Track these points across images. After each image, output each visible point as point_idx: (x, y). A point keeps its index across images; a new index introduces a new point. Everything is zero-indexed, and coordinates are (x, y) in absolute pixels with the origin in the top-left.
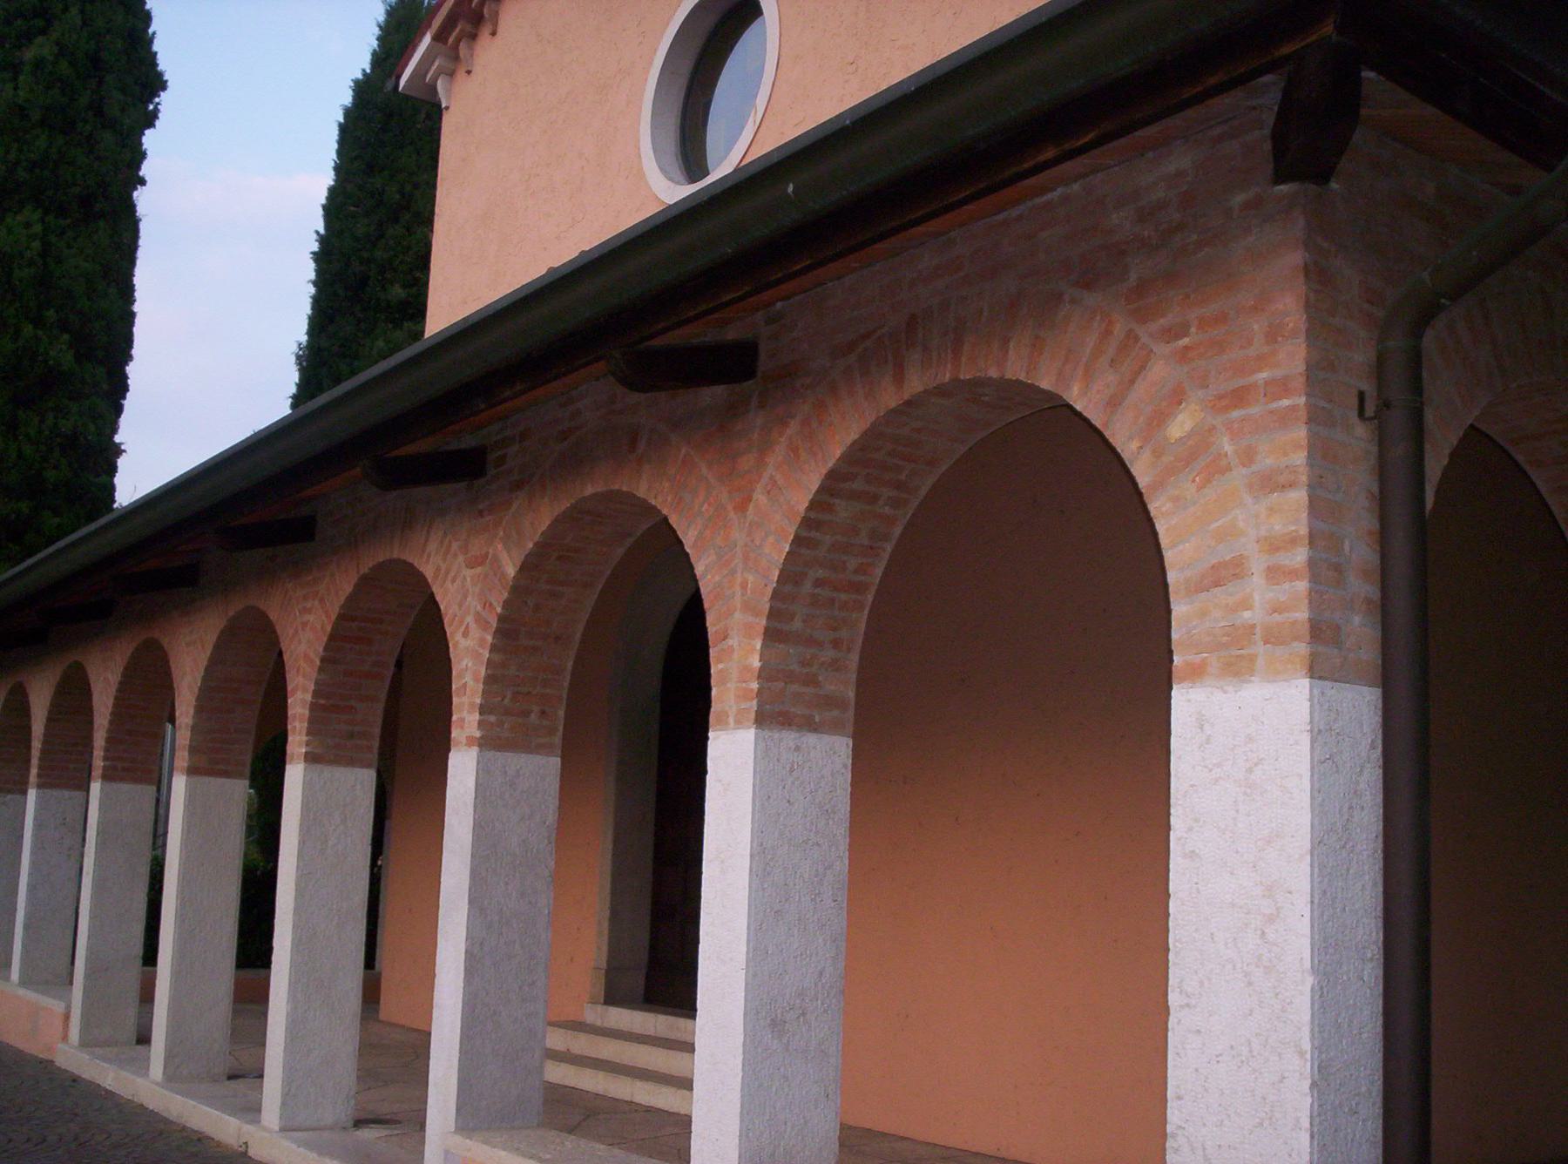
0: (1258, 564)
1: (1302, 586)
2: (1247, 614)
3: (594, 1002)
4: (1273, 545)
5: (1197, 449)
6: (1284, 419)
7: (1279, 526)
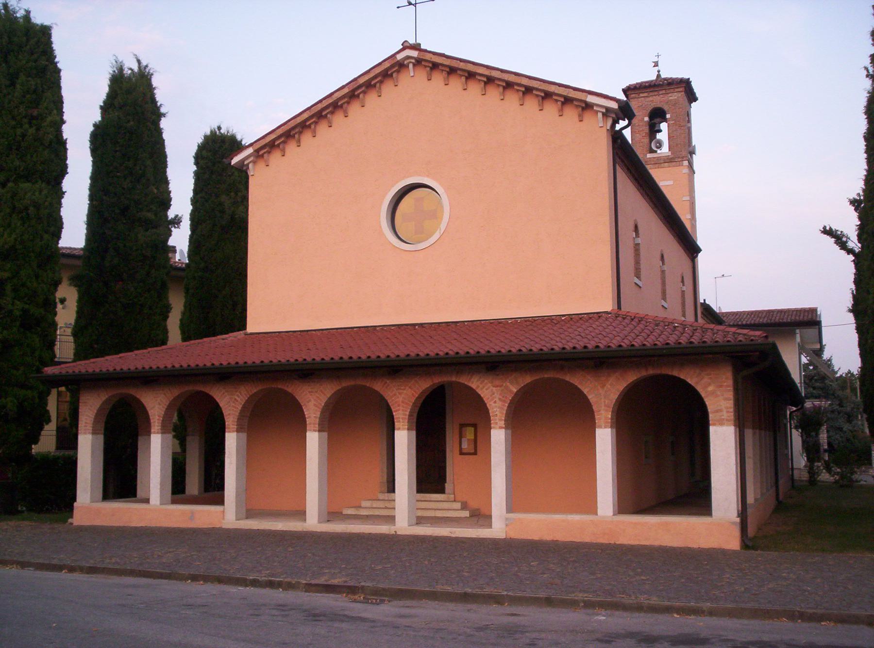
0: (725, 410)
1: (732, 414)
2: (723, 417)
3: (382, 492)
4: (727, 408)
5: (713, 393)
6: (729, 391)
7: (728, 405)
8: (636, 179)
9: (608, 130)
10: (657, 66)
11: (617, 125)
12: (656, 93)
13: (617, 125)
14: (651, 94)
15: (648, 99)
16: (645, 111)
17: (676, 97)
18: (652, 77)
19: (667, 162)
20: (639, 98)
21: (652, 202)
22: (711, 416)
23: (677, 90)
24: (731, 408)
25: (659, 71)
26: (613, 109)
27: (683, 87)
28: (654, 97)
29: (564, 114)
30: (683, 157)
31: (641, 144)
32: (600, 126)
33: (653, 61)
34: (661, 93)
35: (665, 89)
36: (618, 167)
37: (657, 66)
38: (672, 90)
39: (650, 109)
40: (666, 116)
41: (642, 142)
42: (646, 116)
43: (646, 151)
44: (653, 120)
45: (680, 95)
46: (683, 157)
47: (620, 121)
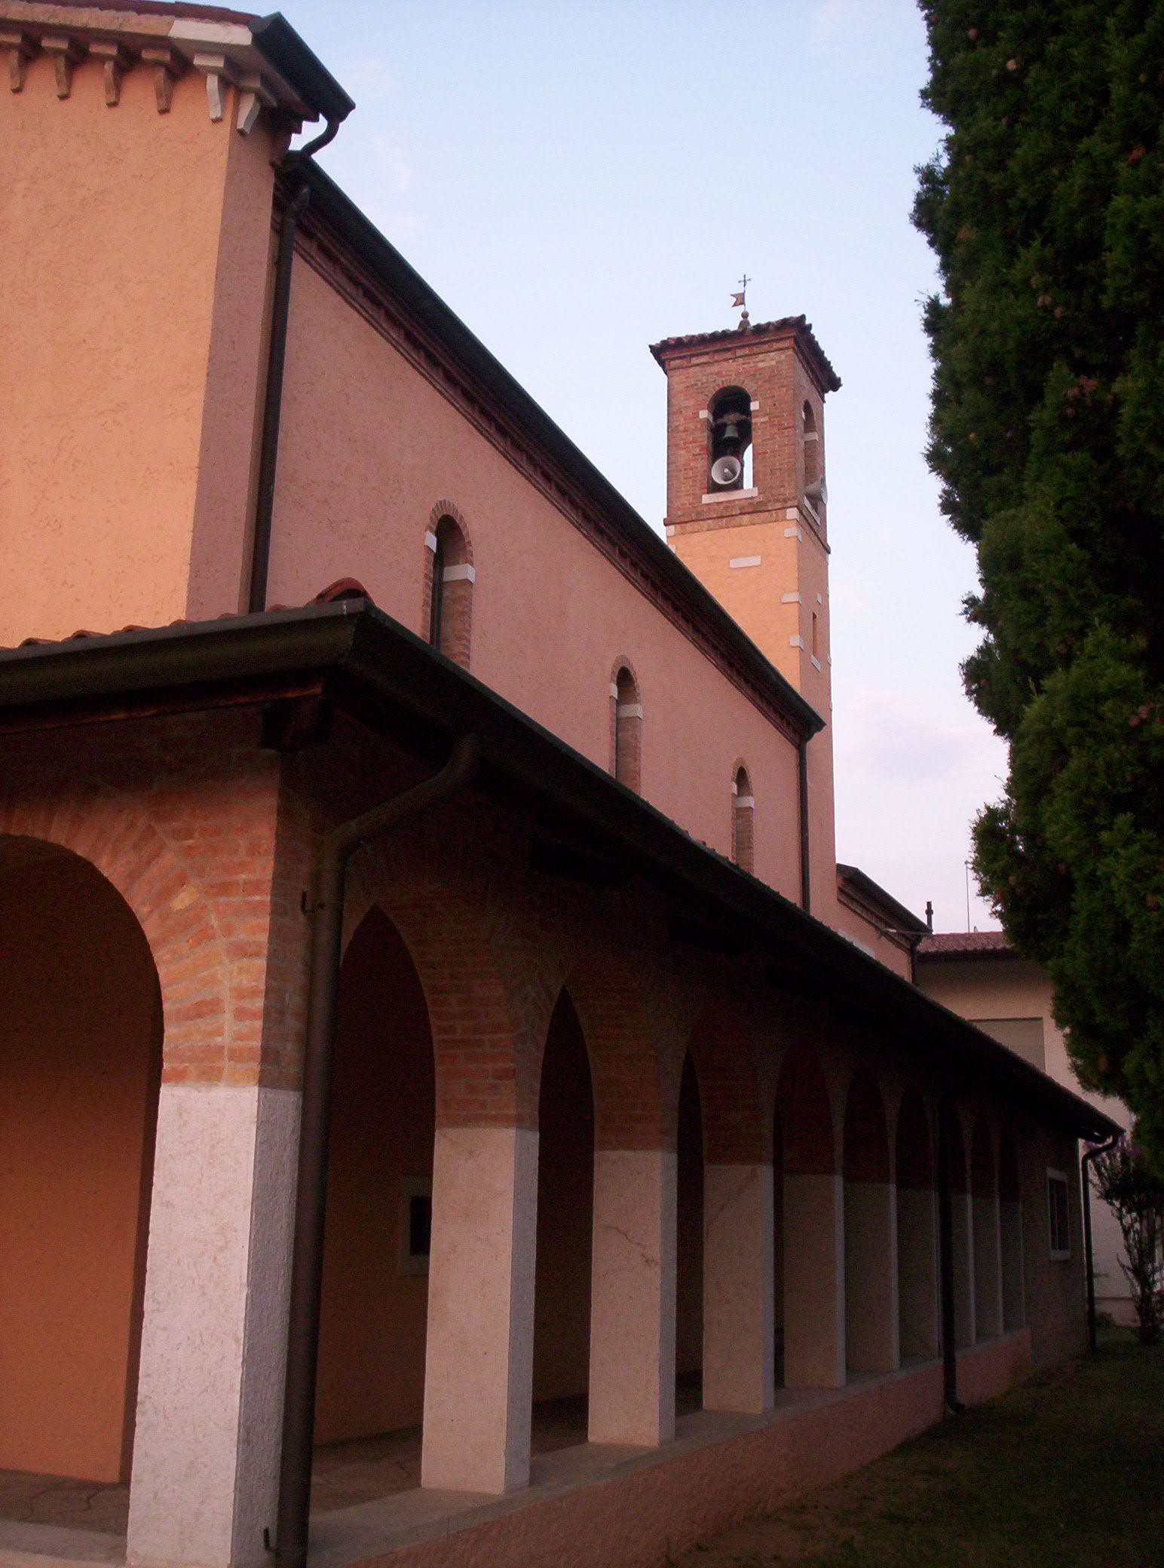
0: (229, 1006)
2: (219, 1039)
4: (240, 993)
6: (254, 909)
7: (245, 981)
8: (470, 399)
9: (241, 132)
10: (743, 303)
11: (294, 136)
12: (729, 355)
13: (294, 136)
14: (717, 357)
15: (709, 369)
16: (701, 397)
17: (774, 363)
18: (733, 326)
19: (749, 513)
20: (690, 367)
21: (573, 504)
22: (170, 1031)
23: (776, 346)
24: (254, 993)
25: (745, 315)
26: (238, 46)
27: (789, 338)
28: (725, 364)
29: (122, 100)
30: (785, 501)
31: (691, 474)
32: (213, 117)
33: (733, 293)
34: (739, 353)
35: (748, 346)
36: (298, 264)
37: (743, 303)
38: (766, 347)
39: (712, 391)
40: (749, 406)
41: (692, 469)
42: (703, 409)
43: (701, 489)
44: (721, 417)
45: (783, 357)
46: (785, 501)
47: (305, 124)
